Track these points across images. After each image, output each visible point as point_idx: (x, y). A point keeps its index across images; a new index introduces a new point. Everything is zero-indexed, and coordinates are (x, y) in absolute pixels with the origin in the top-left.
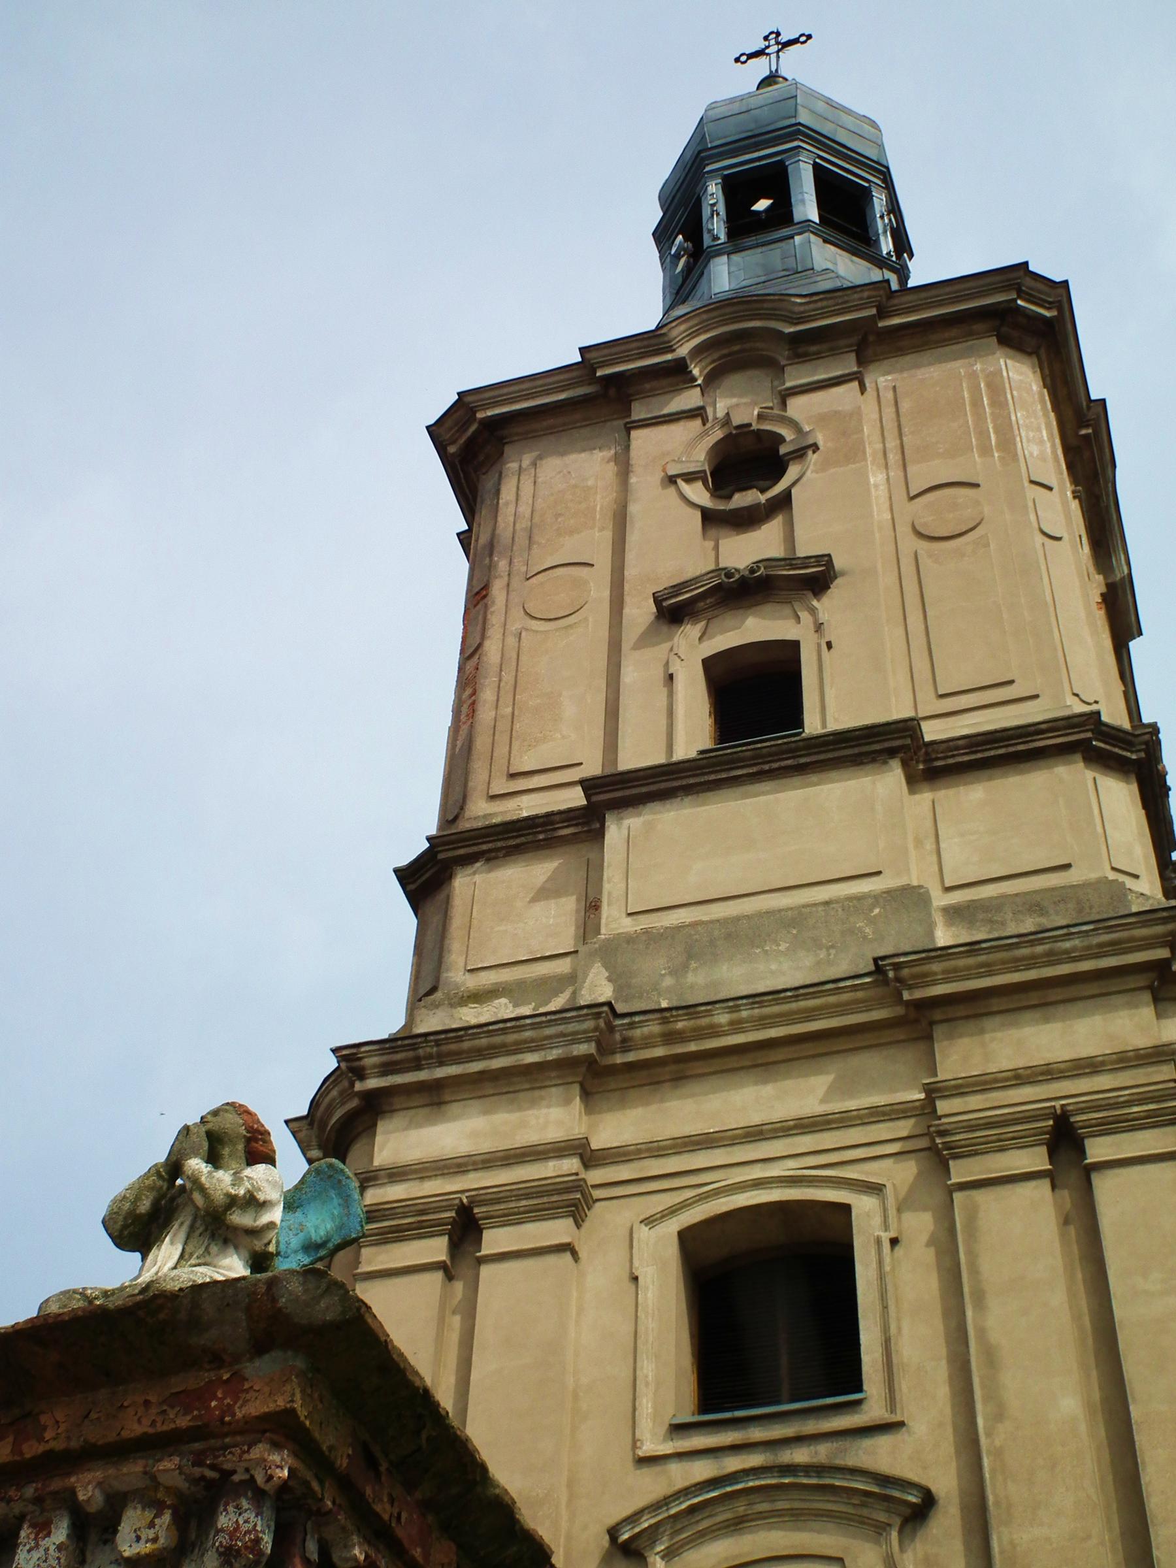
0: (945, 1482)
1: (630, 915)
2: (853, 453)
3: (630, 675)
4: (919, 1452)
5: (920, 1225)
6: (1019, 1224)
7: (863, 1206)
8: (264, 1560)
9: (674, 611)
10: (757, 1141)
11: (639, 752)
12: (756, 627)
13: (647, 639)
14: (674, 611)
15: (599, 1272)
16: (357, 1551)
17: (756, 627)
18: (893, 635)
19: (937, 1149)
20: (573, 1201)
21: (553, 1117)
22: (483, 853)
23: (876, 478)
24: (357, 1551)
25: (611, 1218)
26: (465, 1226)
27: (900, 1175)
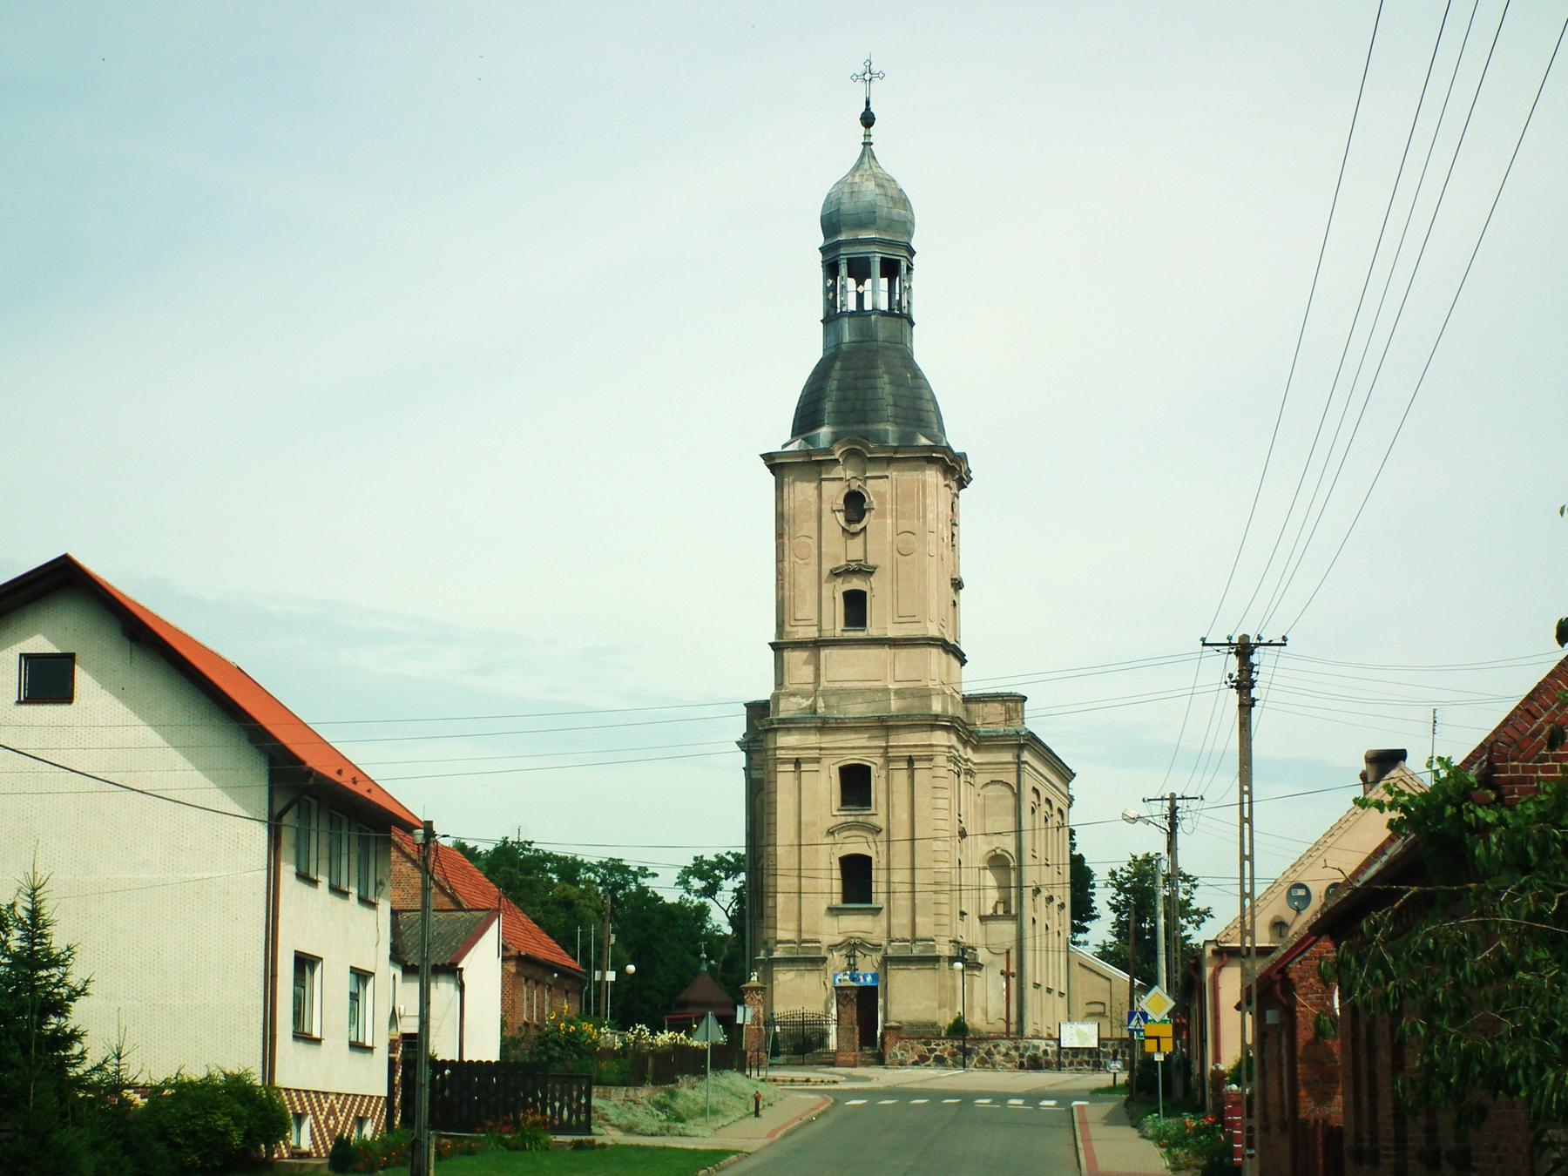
0: (884, 826)
1: (757, 1114)
2: (882, 515)
3: (826, 593)
4: (879, 820)
5: (884, 773)
6: (900, 778)
7: (873, 767)
8: (842, 428)
9: (836, 574)
10: (857, 748)
11: (827, 635)
12: (856, 584)
13: (829, 580)
14: (836, 574)
15: (824, 775)
16: (754, 978)
17: (856, 584)
18: (888, 588)
19: (888, 760)
20: (817, 760)
21: (813, 739)
22: (743, 937)
23: (889, 521)
24: (754, 978)
25: (826, 762)
26: (798, 763)
27: (880, 761)
